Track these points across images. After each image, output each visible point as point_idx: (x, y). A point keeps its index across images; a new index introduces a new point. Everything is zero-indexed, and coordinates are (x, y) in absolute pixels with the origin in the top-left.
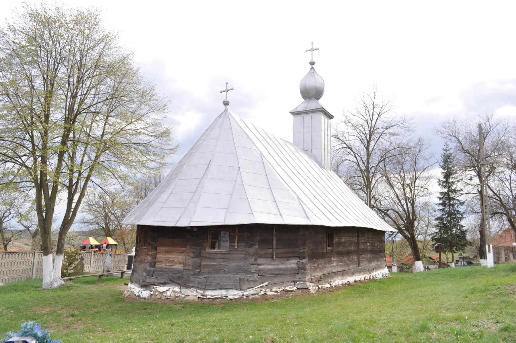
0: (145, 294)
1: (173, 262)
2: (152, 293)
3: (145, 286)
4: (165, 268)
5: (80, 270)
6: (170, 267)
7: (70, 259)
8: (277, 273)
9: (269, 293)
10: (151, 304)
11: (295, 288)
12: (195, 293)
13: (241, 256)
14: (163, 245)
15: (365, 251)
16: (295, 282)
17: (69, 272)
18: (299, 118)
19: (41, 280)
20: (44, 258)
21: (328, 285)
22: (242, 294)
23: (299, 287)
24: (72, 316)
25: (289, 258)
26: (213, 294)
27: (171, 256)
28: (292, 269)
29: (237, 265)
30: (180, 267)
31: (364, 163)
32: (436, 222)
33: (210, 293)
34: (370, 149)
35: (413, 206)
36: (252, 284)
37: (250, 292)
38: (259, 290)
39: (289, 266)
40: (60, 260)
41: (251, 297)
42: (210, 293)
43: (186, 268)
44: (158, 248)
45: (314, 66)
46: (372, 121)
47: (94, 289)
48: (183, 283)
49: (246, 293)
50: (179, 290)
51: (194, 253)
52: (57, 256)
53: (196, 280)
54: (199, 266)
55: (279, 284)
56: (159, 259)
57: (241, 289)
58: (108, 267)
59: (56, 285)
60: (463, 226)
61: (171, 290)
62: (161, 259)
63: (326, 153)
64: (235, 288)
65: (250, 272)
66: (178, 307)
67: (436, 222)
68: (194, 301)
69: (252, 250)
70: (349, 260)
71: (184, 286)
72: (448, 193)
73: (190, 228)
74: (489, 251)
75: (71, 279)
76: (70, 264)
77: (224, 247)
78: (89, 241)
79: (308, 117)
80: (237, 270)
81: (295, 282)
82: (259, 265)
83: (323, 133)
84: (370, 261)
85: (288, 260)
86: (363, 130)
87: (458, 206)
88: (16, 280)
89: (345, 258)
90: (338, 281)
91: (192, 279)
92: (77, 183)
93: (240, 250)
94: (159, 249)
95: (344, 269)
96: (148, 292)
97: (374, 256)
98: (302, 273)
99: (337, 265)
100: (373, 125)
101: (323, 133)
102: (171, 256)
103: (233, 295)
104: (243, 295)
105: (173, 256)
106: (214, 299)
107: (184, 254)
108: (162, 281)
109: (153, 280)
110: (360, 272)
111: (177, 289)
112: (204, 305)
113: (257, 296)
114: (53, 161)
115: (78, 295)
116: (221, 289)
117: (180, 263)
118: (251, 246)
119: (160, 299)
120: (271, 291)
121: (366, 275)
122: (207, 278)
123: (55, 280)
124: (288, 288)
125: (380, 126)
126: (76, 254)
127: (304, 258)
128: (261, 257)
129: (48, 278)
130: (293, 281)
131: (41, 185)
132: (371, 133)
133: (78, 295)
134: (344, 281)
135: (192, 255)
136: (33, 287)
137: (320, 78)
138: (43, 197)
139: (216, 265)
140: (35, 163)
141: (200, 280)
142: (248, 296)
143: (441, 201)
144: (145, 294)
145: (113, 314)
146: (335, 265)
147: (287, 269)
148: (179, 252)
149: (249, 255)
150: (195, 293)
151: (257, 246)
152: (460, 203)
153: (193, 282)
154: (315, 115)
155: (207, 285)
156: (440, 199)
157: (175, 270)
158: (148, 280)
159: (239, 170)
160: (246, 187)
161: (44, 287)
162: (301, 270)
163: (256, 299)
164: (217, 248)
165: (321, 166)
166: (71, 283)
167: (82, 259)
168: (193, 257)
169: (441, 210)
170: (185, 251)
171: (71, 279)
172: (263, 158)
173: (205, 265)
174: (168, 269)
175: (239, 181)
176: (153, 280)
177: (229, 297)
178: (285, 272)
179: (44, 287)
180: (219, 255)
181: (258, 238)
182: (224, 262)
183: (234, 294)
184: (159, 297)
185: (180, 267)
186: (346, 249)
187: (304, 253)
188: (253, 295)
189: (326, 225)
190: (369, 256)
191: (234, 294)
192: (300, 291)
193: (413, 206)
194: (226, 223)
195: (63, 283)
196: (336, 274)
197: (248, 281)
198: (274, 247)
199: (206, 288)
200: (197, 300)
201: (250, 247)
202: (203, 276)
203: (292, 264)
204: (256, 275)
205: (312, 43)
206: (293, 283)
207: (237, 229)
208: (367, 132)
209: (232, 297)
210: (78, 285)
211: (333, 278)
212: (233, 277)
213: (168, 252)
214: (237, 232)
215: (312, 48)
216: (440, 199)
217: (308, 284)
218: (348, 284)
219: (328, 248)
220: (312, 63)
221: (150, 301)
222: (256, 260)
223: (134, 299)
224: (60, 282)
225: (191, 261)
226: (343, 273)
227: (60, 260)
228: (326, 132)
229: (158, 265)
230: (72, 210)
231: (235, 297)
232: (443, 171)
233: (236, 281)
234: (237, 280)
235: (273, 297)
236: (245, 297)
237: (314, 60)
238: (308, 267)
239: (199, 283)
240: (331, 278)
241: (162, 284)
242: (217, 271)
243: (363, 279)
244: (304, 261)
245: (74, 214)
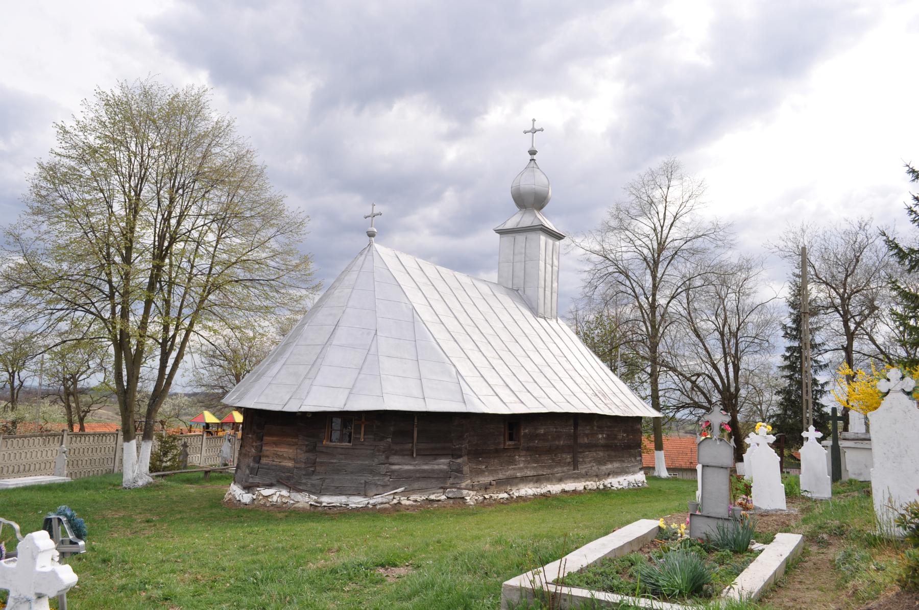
0: (246, 498)
2: (255, 497)
3: (248, 488)
5: (182, 462)
7: (166, 446)
8: (418, 475)
9: (405, 502)
10: (249, 511)
11: (443, 497)
12: (307, 499)
13: (369, 452)
14: (271, 435)
15: (591, 447)
16: (444, 488)
17: (164, 464)
18: (508, 238)
19: (121, 475)
20: (126, 444)
21: (505, 495)
23: (450, 495)
24: (148, 522)
25: (436, 455)
28: (441, 471)
30: (290, 465)
31: (647, 299)
32: (779, 398)
34: (659, 275)
35: (737, 369)
36: (380, 489)
37: (378, 499)
38: (392, 497)
39: (436, 467)
40: (148, 448)
41: (378, 507)
42: (326, 500)
43: (298, 466)
44: (265, 438)
45: (535, 157)
46: (662, 227)
47: (192, 491)
48: (294, 487)
49: (372, 501)
51: (307, 446)
52: (143, 443)
54: (314, 463)
55: (421, 490)
56: (265, 453)
57: (366, 496)
58: (225, 459)
59: (140, 483)
60: (823, 406)
61: (278, 494)
62: (268, 453)
63: (548, 293)
64: (359, 494)
65: (379, 474)
66: (280, 515)
67: (779, 398)
68: (304, 509)
69: (383, 445)
70: (553, 460)
72: (799, 349)
75: (163, 476)
76: (165, 454)
77: (334, 441)
78: (203, 417)
79: (520, 238)
80: (362, 470)
81: (444, 488)
82: (393, 464)
83: (542, 264)
84: (601, 462)
85: (435, 459)
86: (648, 243)
87: (816, 371)
88: (91, 474)
89: (544, 458)
90: (527, 490)
91: (304, 481)
92: (174, 336)
94: (267, 439)
95: (541, 473)
96: (250, 495)
97: (613, 454)
98: (456, 477)
99: (527, 468)
100: (664, 236)
101: (542, 264)
106: (331, 507)
108: (268, 482)
109: (257, 480)
110: (577, 478)
111: (284, 492)
112: (316, 513)
113: (387, 505)
114: (138, 307)
115: (167, 496)
116: (341, 494)
117: (290, 459)
118: (382, 439)
119: (264, 505)
120: (408, 499)
121: (588, 483)
122: (323, 480)
123: (140, 476)
124: (432, 497)
125: (677, 236)
126: (175, 439)
127: (460, 456)
128: (395, 454)
129: (130, 472)
130: (442, 488)
131: (121, 345)
132: (662, 246)
133: (167, 496)
134: (539, 490)
135: (304, 448)
136: (110, 484)
137: (543, 176)
138: (124, 362)
140: (113, 313)
142: (374, 505)
143: (787, 363)
144: (246, 498)
145: (197, 521)
146: (521, 466)
147: (433, 471)
148: (290, 445)
149: (379, 451)
150: (307, 499)
151: (390, 440)
152: (820, 367)
153: (305, 484)
154: (532, 236)
156: (786, 358)
157: (284, 467)
158: (251, 480)
159: (376, 334)
160: (381, 358)
161: (124, 485)
162: (458, 472)
163: (385, 509)
165: (535, 312)
166: (163, 481)
167: (185, 445)
168: (307, 452)
169: (787, 377)
170: (296, 444)
171: (163, 476)
172: (415, 315)
173: (321, 463)
175: (373, 349)
176: (257, 480)
178: (430, 475)
179: (124, 485)
181: (392, 429)
183: (357, 501)
184: (262, 502)
185: (290, 464)
186: (547, 444)
187: (460, 449)
188: (382, 503)
190: (601, 454)
191: (357, 501)
192: (451, 501)
193: (737, 369)
194: (345, 409)
195: (151, 480)
196: (525, 480)
197: (376, 484)
198: (415, 440)
199: (320, 492)
201: (380, 440)
203: (442, 464)
204: (387, 478)
205: (534, 120)
206: (441, 490)
207: (337, 422)
208: (656, 246)
209: (354, 506)
210: (174, 484)
211: (517, 484)
213: (276, 444)
215: (533, 128)
216: (786, 358)
217: (465, 492)
218: (546, 496)
219: (508, 443)
220: (533, 153)
221: (251, 507)
222: (387, 458)
223: (235, 504)
224: (146, 479)
225: (303, 456)
226: (538, 479)
227: (148, 448)
228: (549, 261)
229: (264, 461)
230: (166, 377)
232: (792, 311)
235: (407, 508)
236: (370, 506)
238: (466, 469)
239: (313, 485)
240: (511, 485)
242: (337, 471)
243: (601, 487)
244: (459, 461)
245: (169, 383)
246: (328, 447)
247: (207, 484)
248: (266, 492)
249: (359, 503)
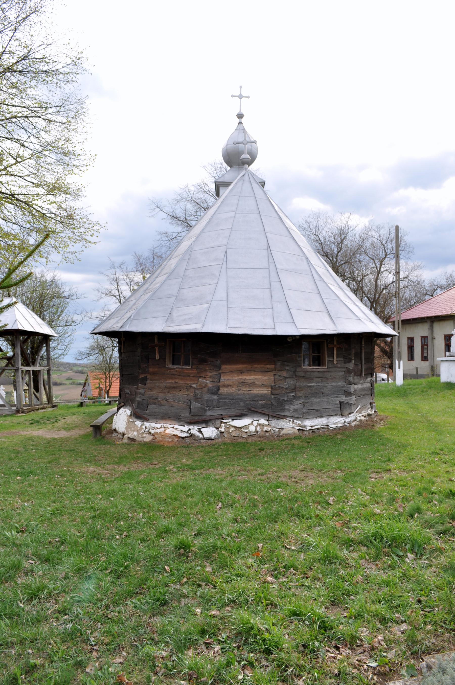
1: (253, 385)
4: (238, 395)
6: (246, 392)
12: (291, 425)
14: (229, 362)
22: (343, 421)
26: (313, 424)
27: (247, 378)
29: (336, 386)
30: (265, 392)
33: (309, 423)
37: (352, 417)
41: (353, 424)
42: (309, 423)
49: (348, 420)
50: (266, 423)
53: (292, 408)
57: (342, 415)
61: (255, 423)
64: (337, 415)
71: (273, 417)
73: (298, 337)
74: (399, 368)
80: (335, 392)
93: (339, 366)
102: (247, 378)
103: (334, 424)
104: (345, 422)
105: (252, 377)
107: (272, 373)
111: (263, 421)
116: (321, 416)
117: (265, 386)
118: (350, 361)
139: (313, 386)
141: (295, 407)
142: (349, 423)
144: (209, 432)
153: (289, 410)
155: (305, 413)
157: (256, 396)
158: (209, 413)
164: (38, 365)
170: (275, 370)
173: (300, 387)
174: (244, 395)
177: (331, 426)
180: (316, 374)
182: (322, 381)
185: (266, 391)
189: (44, 333)
191: (336, 422)
197: (350, 404)
199: (304, 416)
200: (297, 432)
202: (299, 402)
207: (305, 346)
209: (334, 426)
212: (332, 401)
213: (242, 372)
214: (335, 343)
215: (241, 95)
220: (240, 116)
224: (353, 426)
229: (223, 391)
231: (338, 425)
233: (336, 406)
234: (337, 404)
237: (243, 112)
239: (295, 411)
241: (235, 416)
242: (315, 394)
246: (306, 371)
247: (62, 436)
248: (238, 423)
249: (337, 423)
